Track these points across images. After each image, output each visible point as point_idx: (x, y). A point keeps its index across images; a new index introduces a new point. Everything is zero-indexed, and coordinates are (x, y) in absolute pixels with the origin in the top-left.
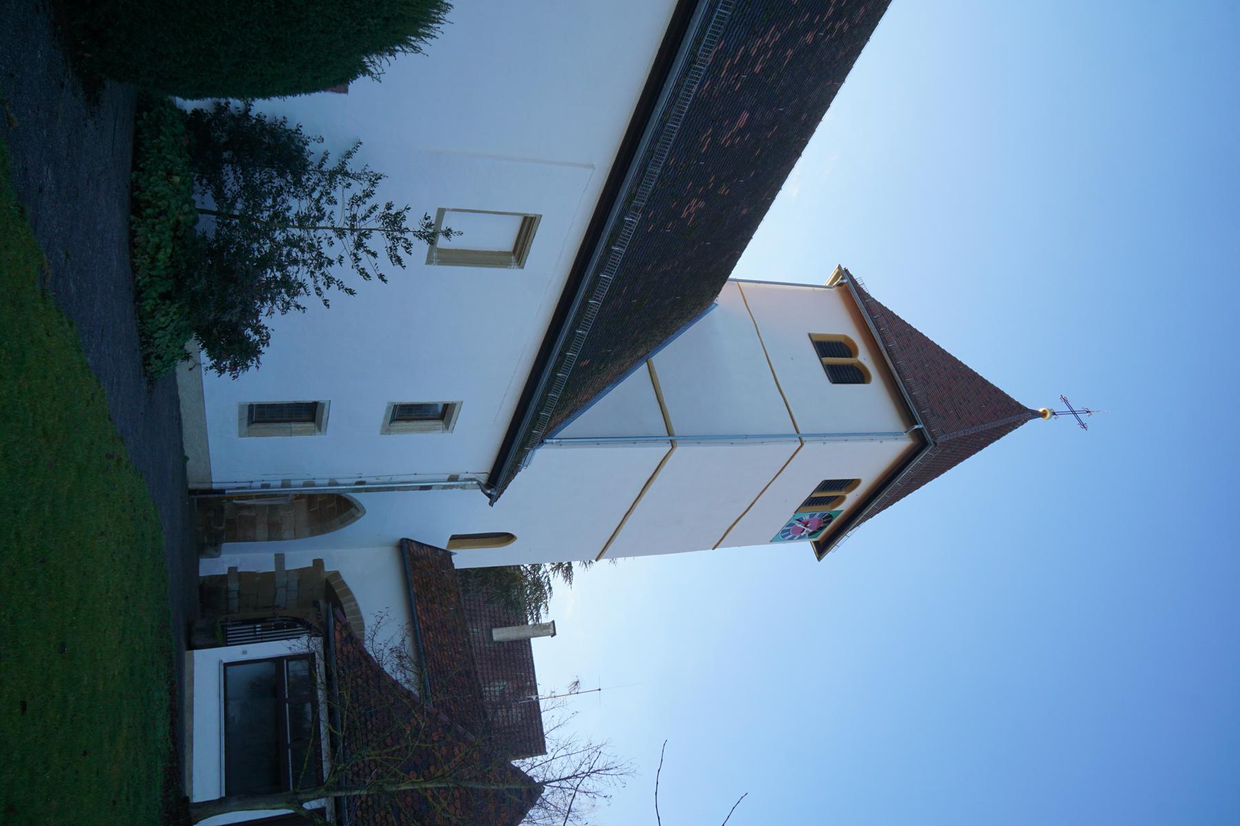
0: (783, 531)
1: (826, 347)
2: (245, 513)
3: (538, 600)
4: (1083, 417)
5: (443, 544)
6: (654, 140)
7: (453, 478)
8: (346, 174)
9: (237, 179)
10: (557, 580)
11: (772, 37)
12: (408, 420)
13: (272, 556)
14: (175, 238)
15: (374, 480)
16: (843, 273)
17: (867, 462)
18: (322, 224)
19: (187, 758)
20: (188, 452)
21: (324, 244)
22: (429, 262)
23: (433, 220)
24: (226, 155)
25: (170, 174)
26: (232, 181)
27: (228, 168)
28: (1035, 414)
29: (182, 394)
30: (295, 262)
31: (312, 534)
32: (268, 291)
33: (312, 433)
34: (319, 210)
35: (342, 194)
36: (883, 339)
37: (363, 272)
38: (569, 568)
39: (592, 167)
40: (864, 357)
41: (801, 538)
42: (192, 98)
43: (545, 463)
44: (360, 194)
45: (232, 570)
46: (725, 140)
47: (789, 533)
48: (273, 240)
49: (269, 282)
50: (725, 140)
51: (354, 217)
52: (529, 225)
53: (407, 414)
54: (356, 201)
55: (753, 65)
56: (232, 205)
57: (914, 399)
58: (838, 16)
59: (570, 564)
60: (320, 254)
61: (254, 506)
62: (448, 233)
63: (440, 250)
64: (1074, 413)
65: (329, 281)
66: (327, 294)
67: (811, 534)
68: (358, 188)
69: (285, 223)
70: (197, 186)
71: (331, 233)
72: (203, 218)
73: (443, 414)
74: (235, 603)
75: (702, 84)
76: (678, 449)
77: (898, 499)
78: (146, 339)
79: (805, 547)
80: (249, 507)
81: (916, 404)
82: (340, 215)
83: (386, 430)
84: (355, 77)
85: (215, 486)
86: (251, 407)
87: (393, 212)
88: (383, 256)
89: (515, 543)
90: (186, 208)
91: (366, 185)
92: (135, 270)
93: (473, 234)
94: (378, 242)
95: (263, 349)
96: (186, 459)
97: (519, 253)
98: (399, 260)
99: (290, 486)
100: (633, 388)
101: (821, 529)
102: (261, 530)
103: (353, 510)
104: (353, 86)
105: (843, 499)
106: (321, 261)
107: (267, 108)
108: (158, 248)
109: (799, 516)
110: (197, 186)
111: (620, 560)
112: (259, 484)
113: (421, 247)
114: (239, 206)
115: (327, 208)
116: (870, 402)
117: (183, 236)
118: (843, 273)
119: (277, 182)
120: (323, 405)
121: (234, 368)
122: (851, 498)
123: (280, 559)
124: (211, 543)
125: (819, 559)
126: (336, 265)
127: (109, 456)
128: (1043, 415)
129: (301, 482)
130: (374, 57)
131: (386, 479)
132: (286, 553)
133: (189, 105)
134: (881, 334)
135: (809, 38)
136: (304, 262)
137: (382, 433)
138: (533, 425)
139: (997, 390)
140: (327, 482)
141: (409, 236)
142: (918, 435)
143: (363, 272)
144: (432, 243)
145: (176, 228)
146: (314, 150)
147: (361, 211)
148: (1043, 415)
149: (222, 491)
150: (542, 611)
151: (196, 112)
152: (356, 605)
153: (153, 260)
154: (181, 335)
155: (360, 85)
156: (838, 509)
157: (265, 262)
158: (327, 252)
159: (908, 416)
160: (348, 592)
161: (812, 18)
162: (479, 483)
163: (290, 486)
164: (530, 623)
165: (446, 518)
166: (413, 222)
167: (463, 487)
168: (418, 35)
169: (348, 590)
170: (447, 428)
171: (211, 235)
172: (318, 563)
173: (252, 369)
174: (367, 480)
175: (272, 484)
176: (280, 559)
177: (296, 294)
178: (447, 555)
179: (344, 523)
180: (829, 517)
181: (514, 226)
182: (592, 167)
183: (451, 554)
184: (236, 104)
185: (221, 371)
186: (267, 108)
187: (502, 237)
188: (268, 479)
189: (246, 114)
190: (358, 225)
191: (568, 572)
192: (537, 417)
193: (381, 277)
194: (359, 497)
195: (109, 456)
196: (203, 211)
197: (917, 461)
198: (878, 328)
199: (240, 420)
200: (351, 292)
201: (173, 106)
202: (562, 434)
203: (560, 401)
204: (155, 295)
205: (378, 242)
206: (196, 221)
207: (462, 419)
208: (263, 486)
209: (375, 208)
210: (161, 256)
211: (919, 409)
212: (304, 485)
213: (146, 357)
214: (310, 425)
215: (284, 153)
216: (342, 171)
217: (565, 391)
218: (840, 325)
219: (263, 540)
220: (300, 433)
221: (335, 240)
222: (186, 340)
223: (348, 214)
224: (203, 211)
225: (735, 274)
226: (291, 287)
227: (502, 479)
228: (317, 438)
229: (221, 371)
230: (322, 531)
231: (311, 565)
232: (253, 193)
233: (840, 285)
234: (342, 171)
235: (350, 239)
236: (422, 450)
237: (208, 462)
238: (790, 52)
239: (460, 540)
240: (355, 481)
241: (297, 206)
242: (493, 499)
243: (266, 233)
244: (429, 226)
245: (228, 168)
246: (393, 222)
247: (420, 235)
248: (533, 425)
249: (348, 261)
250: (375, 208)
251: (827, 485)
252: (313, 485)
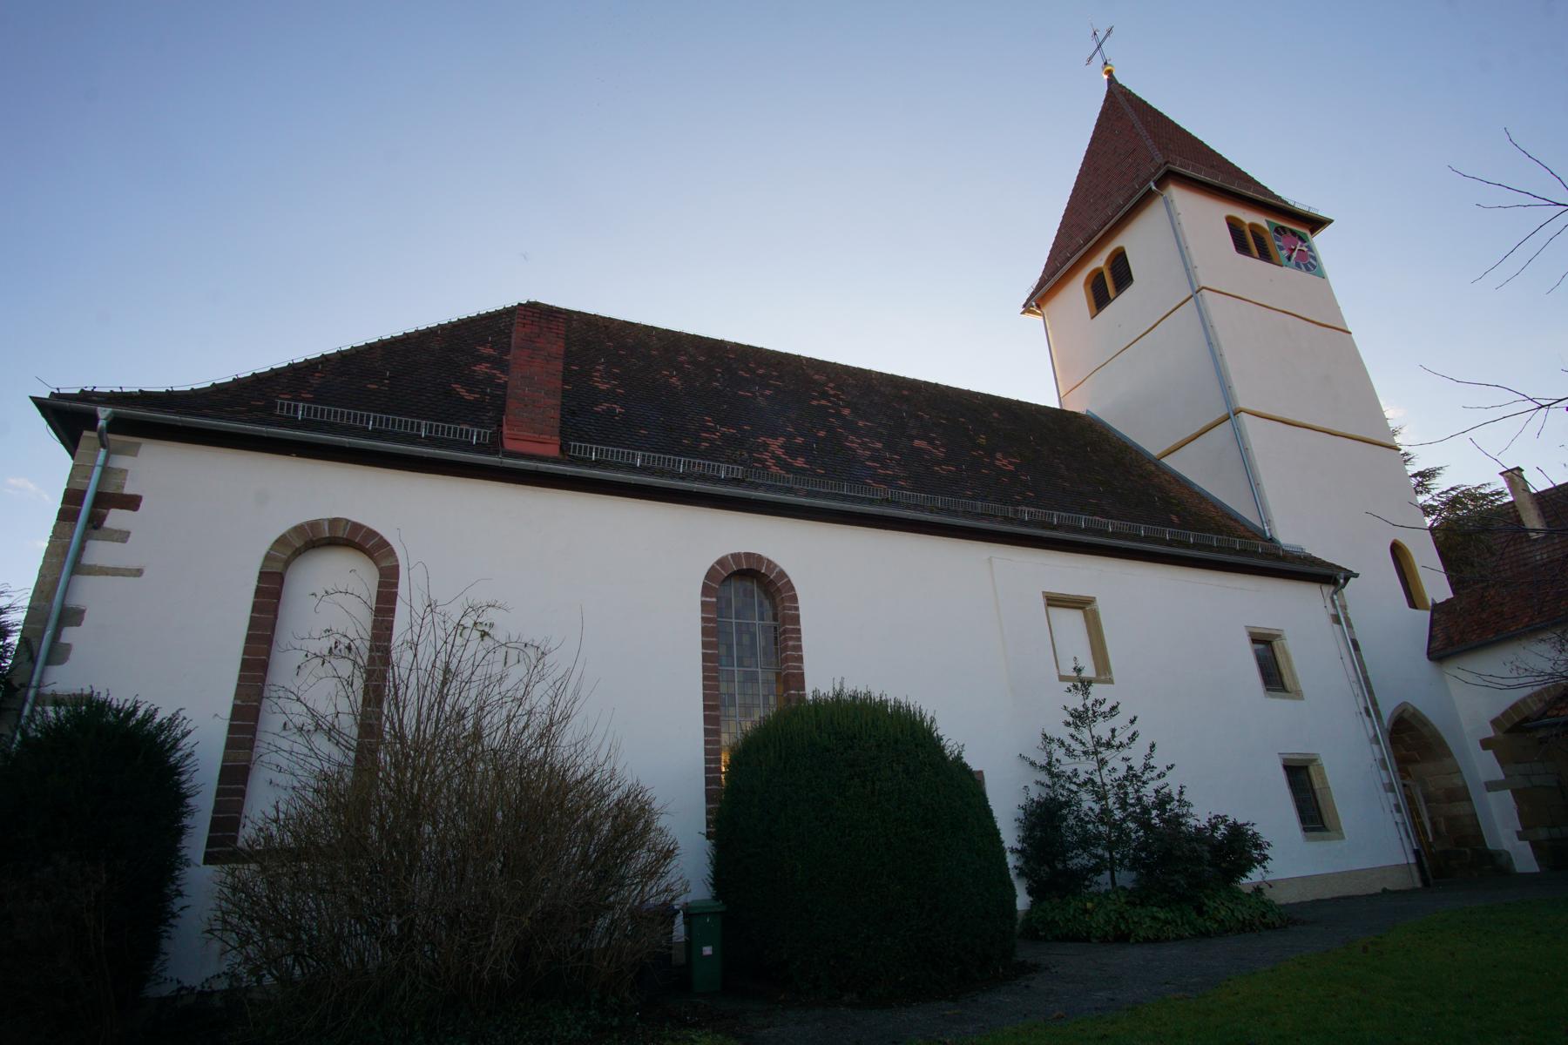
0: (1308, 270)
1: (1099, 299)
2: (1443, 828)
3: (1473, 498)
4: (1101, 36)
5: (1425, 616)
6: (955, 513)
7: (1336, 619)
8: (1049, 763)
9: (1077, 856)
10: (1441, 484)
11: (853, 442)
12: (1281, 675)
13: (1491, 796)
14: (1142, 904)
15: (1360, 700)
16: (1027, 308)
17: (1199, 218)
18: (1098, 780)
20: (1378, 889)
21: (1116, 775)
22: (1111, 681)
23: (1070, 684)
24: (1060, 866)
25: (1086, 911)
26: (1080, 860)
27: (1070, 864)
28: (1112, 80)
29: (1310, 897)
30: (1139, 799)
31: (1450, 755)
32: (1175, 821)
33: (1320, 767)
34: (1085, 783)
35: (1067, 765)
36: (1078, 250)
37: (1133, 738)
38: (1421, 474)
39: (990, 559)
40: (1100, 261)
41: (1310, 249)
42: (1014, 896)
43: (1291, 531)
44: (1063, 750)
45: (1521, 836)
46: (940, 453)
47: (1308, 263)
48: (1124, 820)
49: (1163, 821)
50: (940, 453)
51: (1085, 753)
52: (1053, 601)
53: (1273, 675)
54: (1070, 752)
55: (878, 450)
56: (1101, 857)
57: (1127, 201)
58: (824, 395)
59: (1414, 476)
60: (1125, 778)
61: (1431, 819)
62: (1078, 670)
63: (1098, 674)
64: (1099, 46)
65: (1147, 767)
66: (1161, 768)
67: (1303, 240)
68: (1059, 753)
69: (1105, 811)
70: (1094, 889)
71: (1105, 771)
72: (1119, 883)
73: (1266, 647)
75: (902, 488)
76: (1242, 404)
77: (1238, 170)
78: (1246, 927)
79: (1320, 242)
80: (1434, 824)
81: (1131, 196)
82: (1086, 766)
83: (1298, 695)
84: (965, 765)
85: (1412, 860)
86: (1305, 830)
87: (1070, 719)
88: (1115, 722)
89: (1402, 540)
90: (1112, 896)
91: (1055, 746)
92: (1180, 938)
93: (1077, 650)
94: (1102, 729)
95: (1231, 820)
97: (1081, 604)
98: (1113, 708)
100: (1190, 466)
101: (1294, 233)
103: (1406, 715)
104: (975, 767)
105: (1253, 226)
106: (1131, 776)
107: (1010, 836)
108: (1154, 918)
109: (1284, 261)
110: (1094, 889)
111: (1392, 425)
113: (1097, 691)
114: (1100, 851)
115: (1083, 777)
116: (1141, 241)
117: (1139, 897)
118: (1027, 308)
119: (1071, 821)
121: (1259, 846)
122: (1248, 217)
123: (1492, 786)
124: (1494, 866)
125: (1331, 221)
126: (1131, 763)
127: (1365, 949)
128: (1109, 73)
129: (1383, 773)
130: (947, 752)
131: (1356, 686)
133: (1023, 901)
134: (1073, 254)
135: (846, 412)
136: (1137, 791)
137: (1302, 698)
138: (1254, 554)
139: (1097, 126)
140: (1375, 747)
141: (1089, 703)
142: (1161, 183)
143: (1133, 738)
144: (1090, 682)
145: (1134, 904)
146: (1036, 793)
147: (1078, 748)
148: (1109, 73)
149: (1416, 853)
150: (1487, 491)
151: (1030, 892)
153: (1167, 922)
154: (1236, 896)
155: (973, 762)
156: (1265, 226)
157: (1145, 824)
158: (1122, 772)
159: (1147, 198)
161: (832, 415)
162: (1335, 592)
164: (1510, 498)
165: (1390, 622)
166: (1076, 701)
167: (1344, 607)
168: (922, 721)
170: (1279, 636)
171: (1134, 875)
172: (1486, 744)
173: (1256, 829)
175: (1393, 801)
176: (1492, 786)
177: (1169, 795)
178: (1437, 608)
179: (1425, 722)
180: (1278, 231)
181: (1059, 614)
182: (990, 559)
183: (1435, 605)
184: (1011, 860)
185: (1266, 858)
186: (1010, 836)
187: (1072, 621)
189: (1021, 852)
190: (1091, 749)
191: (1426, 475)
192: (1243, 552)
193: (1132, 722)
194: (1387, 711)
195: (1365, 949)
196: (1114, 883)
197: (1189, 172)
198: (1068, 259)
200: (1153, 746)
201: (1028, 913)
202: (1258, 523)
203: (1220, 532)
204: (1200, 920)
205: (1102, 729)
206: (1123, 888)
207: (1266, 624)
208: (1398, 809)
209: (1072, 736)
210: (1162, 915)
211: (1135, 192)
212: (1385, 768)
213: (1267, 927)
214: (1312, 770)
215: (1045, 818)
216: (1048, 768)
217: (1209, 531)
218: (1076, 293)
219: (1472, 805)
220: (1324, 779)
221: (1110, 766)
222: (1240, 892)
223: (1083, 758)
224: (1114, 883)
225: (1053, 402)
226: (1163, 801)
227: (1328, 572)
229: (1266, 858)
232: (1086, 842)
233: (1038, 307)
234: (1048, 768)
235: (1106, 754)
236: (1299, 656)
238: (861, 424)
239: (1413, 597)
240: (1367, 719)
241: (1087, 802)
242: (1349, 575)
243: (1117, 826)
244: (1075, 687)
245: (1070, 864)
246: (1080, 718)
247: (1086, 694)
248: (1254, 554)
249: (1125, 753)
250: (1072, 736)
251: (1241, 246)
252: (1383, 760)
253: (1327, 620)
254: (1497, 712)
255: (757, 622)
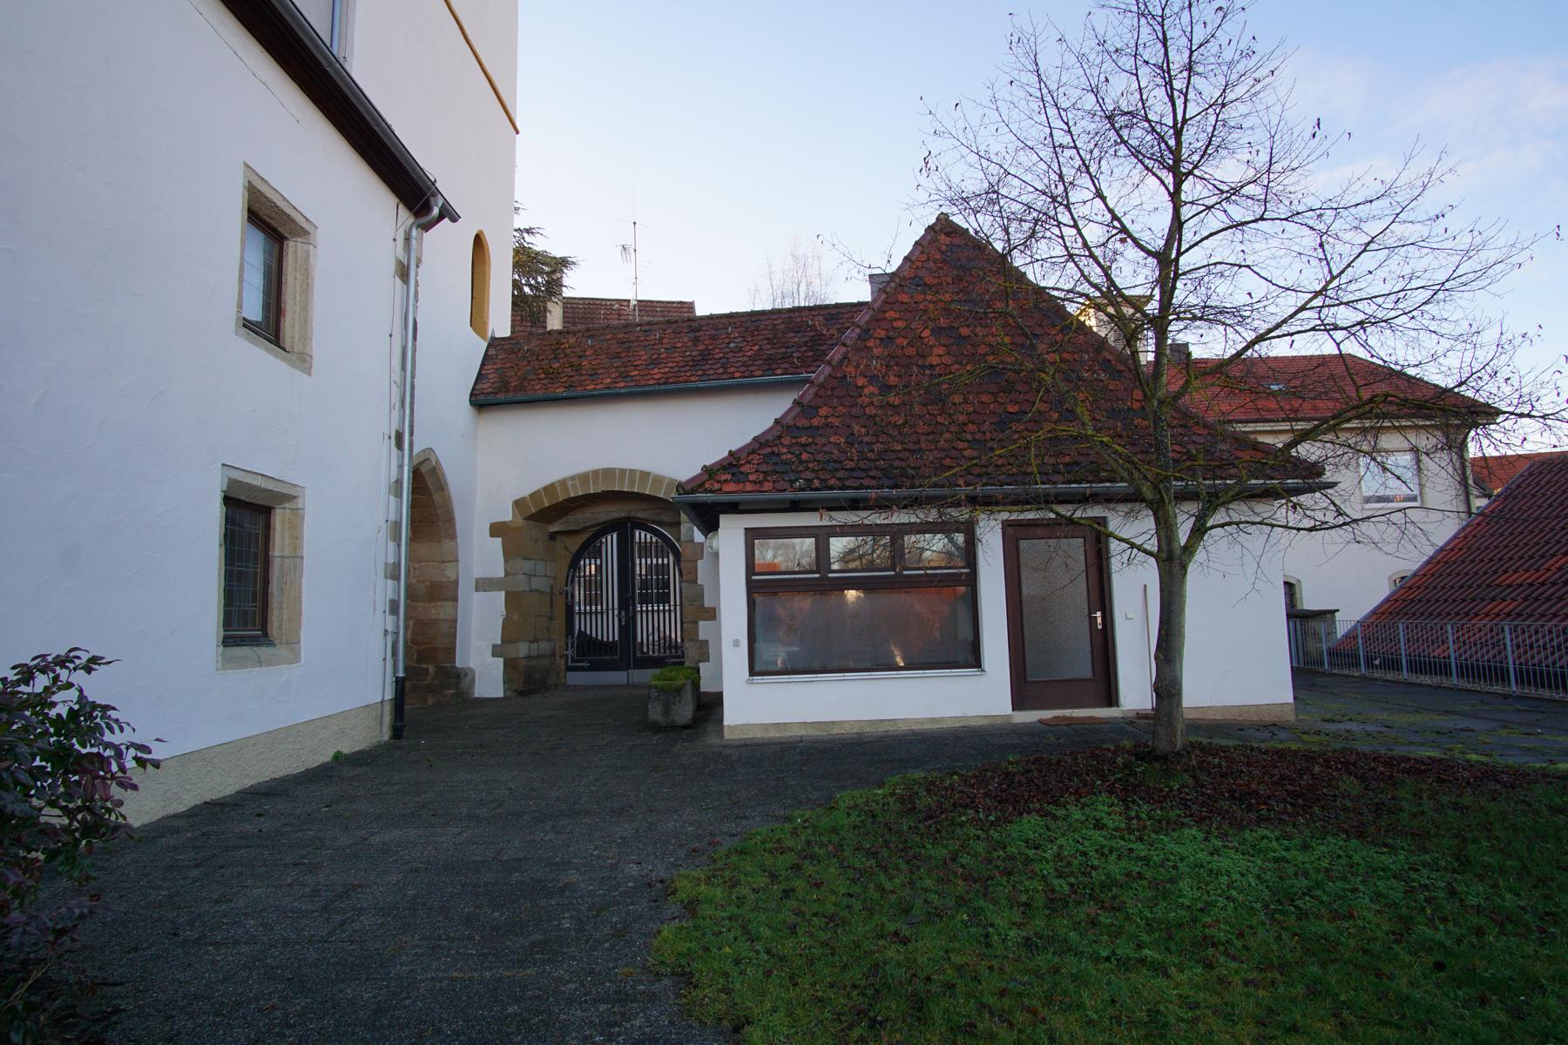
7: (403, 272)
15: (396, 414)
19: (904, 727)
20: (326, 756)
33: (298, 513)
74: (544, 646)
83: (303, 361)
85: (389, 695)
86: (228, 642)
96: (338, 756)
99: (397, 566)
102: (441, 611)
103: (424, 469)
112: (390, 619)
120: (232, 483)
123: (484, 585)
124: (455, 679)
129: (392, 545)
131: (396, 392)
132: (476, 575)
149: (400, 684)
152: (572, 478)
160: (549, 489)
163: (397, 566)
169: (545, 488)
170: (305, 233)
172: (496, 529)
174: (395, 426)
176: (484, 585)
178: (494, 343)
179: (442, 487)
188: (382, 604)
199: (260, 663)
214: (279, 518)
219: (456, 608)
220: (297, 538)
228: (310, 504)
230: (450, 519)
231: (499, 540)
237: (345, 715)
253: (391, 268)
254: (525, 492)
255: (665, 933)
